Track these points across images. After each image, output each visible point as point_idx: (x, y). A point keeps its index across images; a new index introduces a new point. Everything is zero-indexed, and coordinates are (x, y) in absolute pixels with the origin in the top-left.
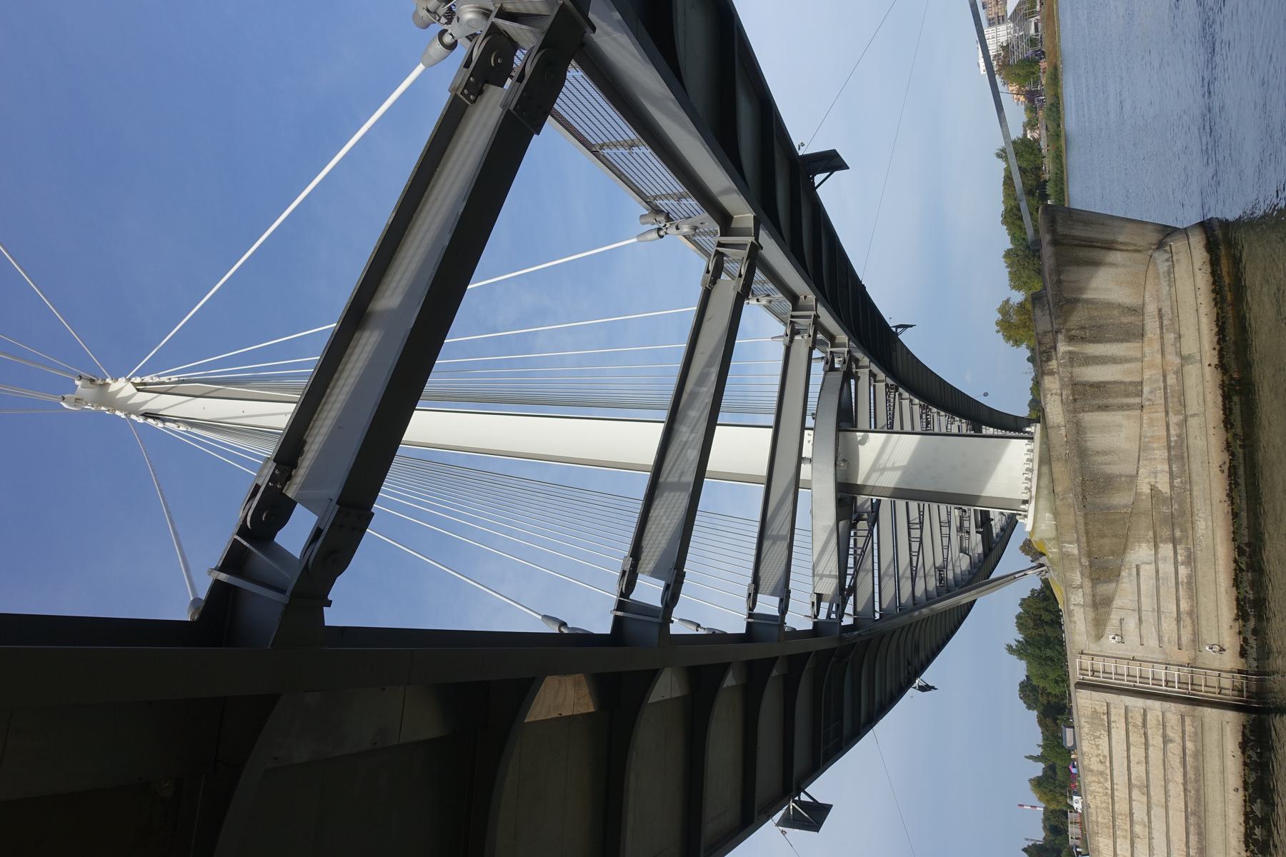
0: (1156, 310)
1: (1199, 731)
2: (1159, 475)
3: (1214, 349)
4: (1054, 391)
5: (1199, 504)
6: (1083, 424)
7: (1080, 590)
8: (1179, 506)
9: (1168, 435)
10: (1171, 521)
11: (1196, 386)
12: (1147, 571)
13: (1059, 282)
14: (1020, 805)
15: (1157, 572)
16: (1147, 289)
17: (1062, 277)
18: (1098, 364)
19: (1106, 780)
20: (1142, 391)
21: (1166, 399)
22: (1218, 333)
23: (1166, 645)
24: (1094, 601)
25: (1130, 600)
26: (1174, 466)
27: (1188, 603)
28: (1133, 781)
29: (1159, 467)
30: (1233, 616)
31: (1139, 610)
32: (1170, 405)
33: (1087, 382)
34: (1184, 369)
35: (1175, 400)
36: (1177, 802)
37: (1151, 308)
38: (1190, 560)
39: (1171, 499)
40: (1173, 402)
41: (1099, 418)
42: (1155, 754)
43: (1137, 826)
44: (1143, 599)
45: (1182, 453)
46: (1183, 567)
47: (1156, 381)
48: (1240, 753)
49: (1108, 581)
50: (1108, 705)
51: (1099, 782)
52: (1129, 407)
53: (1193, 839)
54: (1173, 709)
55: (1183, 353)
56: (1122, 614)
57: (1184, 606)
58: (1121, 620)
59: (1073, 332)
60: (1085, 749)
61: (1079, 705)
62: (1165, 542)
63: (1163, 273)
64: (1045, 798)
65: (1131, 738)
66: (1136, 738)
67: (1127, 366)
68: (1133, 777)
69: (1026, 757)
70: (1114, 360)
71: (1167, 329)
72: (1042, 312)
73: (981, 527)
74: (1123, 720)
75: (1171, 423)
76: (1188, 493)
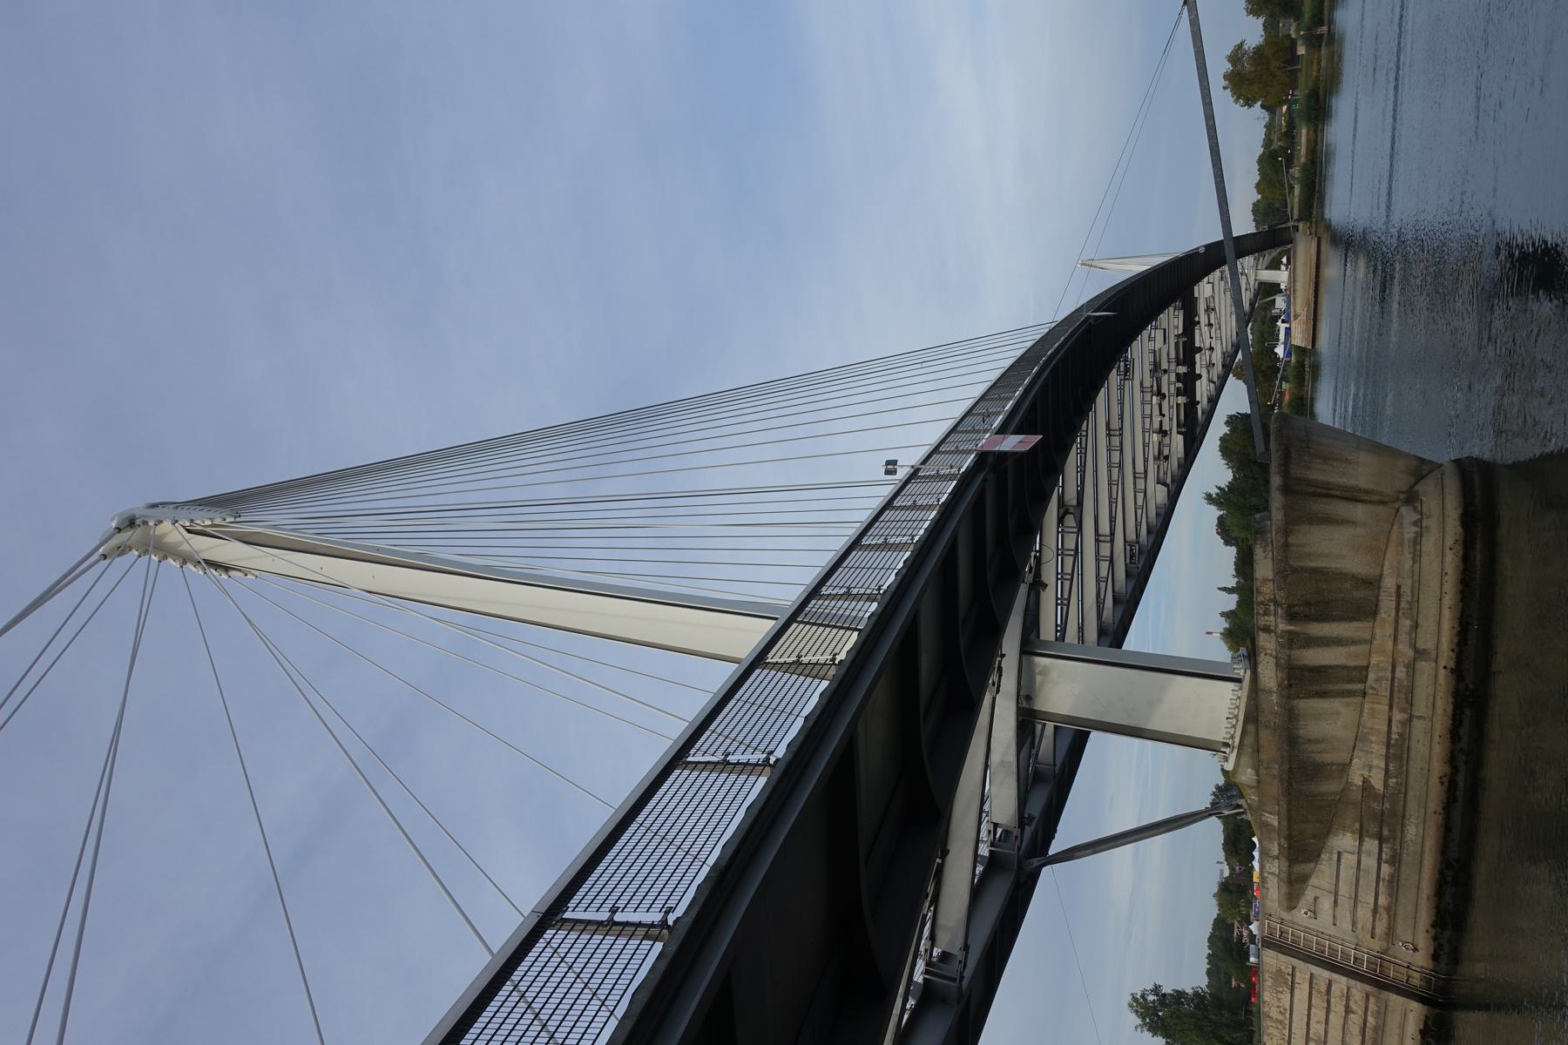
0: (1394, 587)
1: (1382, 1011)
2: (1374, 770)
3: (1453, 650)
4: (1268, 651)
5: (1413, 809)
6: (1296, 711)
7: (1277, 861)
8: (1390, 805)
9: (1389, 732)
10: (1381, 818)
11: (1427, 687)
12: (1349, 860)
13: (1286, 545)
14: (1208, 633)
15: (1359, 862)
16: (1387, 556)
18: (1319, 646)
19: (1285, 1028)
20: (1367, 677)
23: (1359, 931)
26: (1391, 765)
27: (1387, 899)
28: (1311, 1035)
29: (1375, 762)
31: (1336, 894)
32: (1396, 700)
33: (1306, 666)
35: (1401, 696)
37: (1389, 583)
38: (1395, 860)
39: (1383, 797)
40: (1399, 698)
41: (1316, 705)
42: (1336, 1019)
44: (1341, 885)
45: (1402, 754)
46: (1386, 865)
47: (1383, 670)
48: (1419, 1037)
50: (1293, 968)
51: (1277, 1028)
52: (1350, 694)
54: (1359, 990)
55: (1417, 645)
56: (1318, 892)
57: (1382, 901)
58: (1316, 899)
59: (1296, 609)
60: (1266, 999)
62: (1372, 837)
67: (1353, 648)
68: (1311, 1032)
69: (1220, 589)
71: (1403, 613)
72: (1264, 552)
73: (1184, 426)
74: (1307, 985)
75: (1394, 720)
76: (1403, 795)
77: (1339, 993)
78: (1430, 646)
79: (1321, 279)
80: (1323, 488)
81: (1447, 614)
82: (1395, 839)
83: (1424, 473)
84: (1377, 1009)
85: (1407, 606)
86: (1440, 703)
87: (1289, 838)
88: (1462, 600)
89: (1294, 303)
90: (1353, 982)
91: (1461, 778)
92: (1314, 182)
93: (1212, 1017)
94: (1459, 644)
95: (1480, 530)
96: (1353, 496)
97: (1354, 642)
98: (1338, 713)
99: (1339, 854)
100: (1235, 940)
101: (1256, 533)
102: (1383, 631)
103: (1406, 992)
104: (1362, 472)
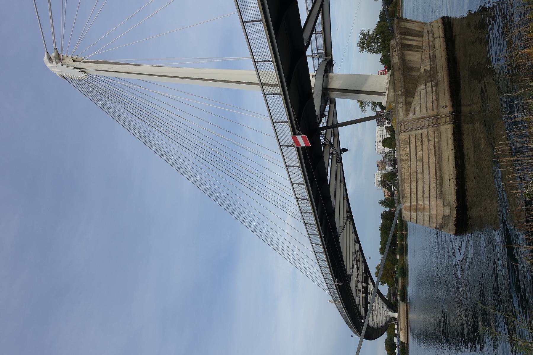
1: (440, 134)
10: (430, 76)
15: (426, 91)
20: (422, 48)
24: (406, 103)
25: (418, 101)
28: (418, 159)
31: (420, 103)
34: (435, 41)
36: (432, 161)
38: (436, 85)
42: (425, 147)
43: (419, 175)
44: (422, 100)
46: (434, 87)
49: (411, 97)
50: (410, 135)
52: (418, 51)
53: (438, 172)
56: (415, 106)
57: (434, 98)
61: (400, 139)
65: (417, 144)
66: (419, 143)
67: (418, 42)
70: (414, 40)
74: (415, 139)
77: (425, 136)
79: (408, 317)
84: (437, 134)
87: (405, 88)
88: (444, 25)
89: (400, 323)
92: (404, 295)
97: (419, 41)
98: (416, 55)
102: (425, 38)
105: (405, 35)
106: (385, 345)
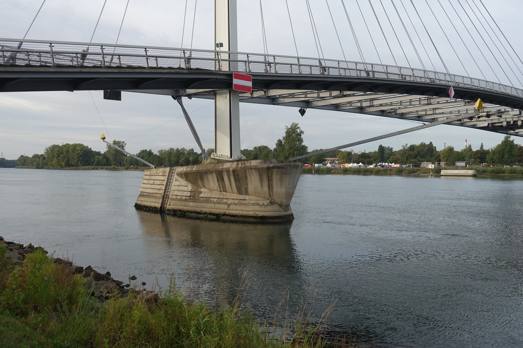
0: (246, 199)
1: (159, 198)
3: (229, 213)
5: (196, 204)
8: (197, 199)
9: (212, 198)
10: (194, 196)
15: (186, 191)
17: (253, 170)
20: (224, 192)
21: (221, 198)
22: (233, 215)
30: (174, 208)
31: (180, 186)
32: (219, 199)
35: (220, 202)
37: (247, 197)
38: (186, 200)
40: (219, 200)
44: (181, 187)
50: (166, 176)
52: (220, 187)
53: (146, 194)
54: (162, 192)
57: (178, 197)
58: (179, 181)
59: (236, 172)
63: (259, 202)
64: (445, 153)
69: (482, 144)
70: (231, 184)
72: (259, 163)
73: (492, 126)
77: (162, 187)
78: (231, 208)
80: (271, 179)
81: (238, 212)
82: (190, 200)
83: (282, 207)
85: (241, 202)
86: (218, 210)
90: (164, 190)
91: (201, 215)
93: (296, 152)
94: (231, 215)
95: (260, 220)
96: (270, 187)
97: (231, 188)
99: (187, 186)
100: (324, 159)
101: (265, 160)
103: (163, 203)
104: (279, 190)
105: (234, 175)
106: (373, 152)
